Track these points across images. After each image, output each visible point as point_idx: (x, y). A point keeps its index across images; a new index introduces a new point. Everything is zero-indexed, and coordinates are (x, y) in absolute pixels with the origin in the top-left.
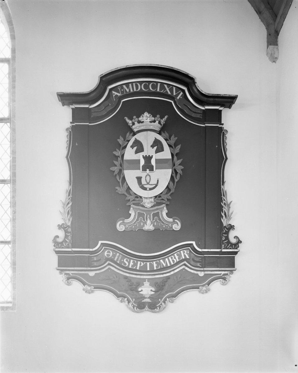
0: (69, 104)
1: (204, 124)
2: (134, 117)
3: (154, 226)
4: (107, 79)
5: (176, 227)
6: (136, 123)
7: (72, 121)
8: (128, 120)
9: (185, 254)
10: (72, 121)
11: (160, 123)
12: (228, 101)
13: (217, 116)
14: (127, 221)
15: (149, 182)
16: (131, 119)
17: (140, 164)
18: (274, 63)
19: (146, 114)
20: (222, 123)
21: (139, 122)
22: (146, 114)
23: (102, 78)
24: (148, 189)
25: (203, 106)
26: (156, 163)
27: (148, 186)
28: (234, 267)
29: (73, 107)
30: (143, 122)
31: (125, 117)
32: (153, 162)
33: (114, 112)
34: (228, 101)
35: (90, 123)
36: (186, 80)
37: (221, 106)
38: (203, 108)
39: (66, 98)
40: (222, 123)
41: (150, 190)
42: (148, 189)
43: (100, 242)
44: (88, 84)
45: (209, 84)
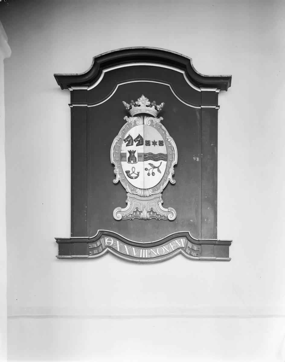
0: (67, 88)
1: (200, 106)
2: (132, 101)
3: (150, 214)
4: (101, 62)
5: (171, 216)
6: (133, 106)
7: (70, 103)
8: (125, 103)
9: (181, 242)
10: (70, 103)
11: (156, 108)
12: (223, 83)
13: (213, 99)
14: (123, 210)
15: (134, 172)
16: (129, 103)
17: (126, 157)
18: (232, 249)
19: (143, 97)
20: (218, 105)
21: (135, 105)
22: (143, 97)
23: (96, 59)
24: (134, 178)
25: (199, 88)
26: (138, 156)
27: (133, 175)
28: (228, 257)
29: (71, 89)
30: (139, 106)
31: (122, 101)
32: (136, 155)
33: (114, 90)
34: (223, 83)
35: (88, 105)
36: (183, 62)
37: (218, 89)
38: (200, 91)
39: (65, 81)
40: (218, 105)
41: (135, 178)
42: (134, 178)
43: (98, 230)
44: (81, 65)
45: (204, 67)
